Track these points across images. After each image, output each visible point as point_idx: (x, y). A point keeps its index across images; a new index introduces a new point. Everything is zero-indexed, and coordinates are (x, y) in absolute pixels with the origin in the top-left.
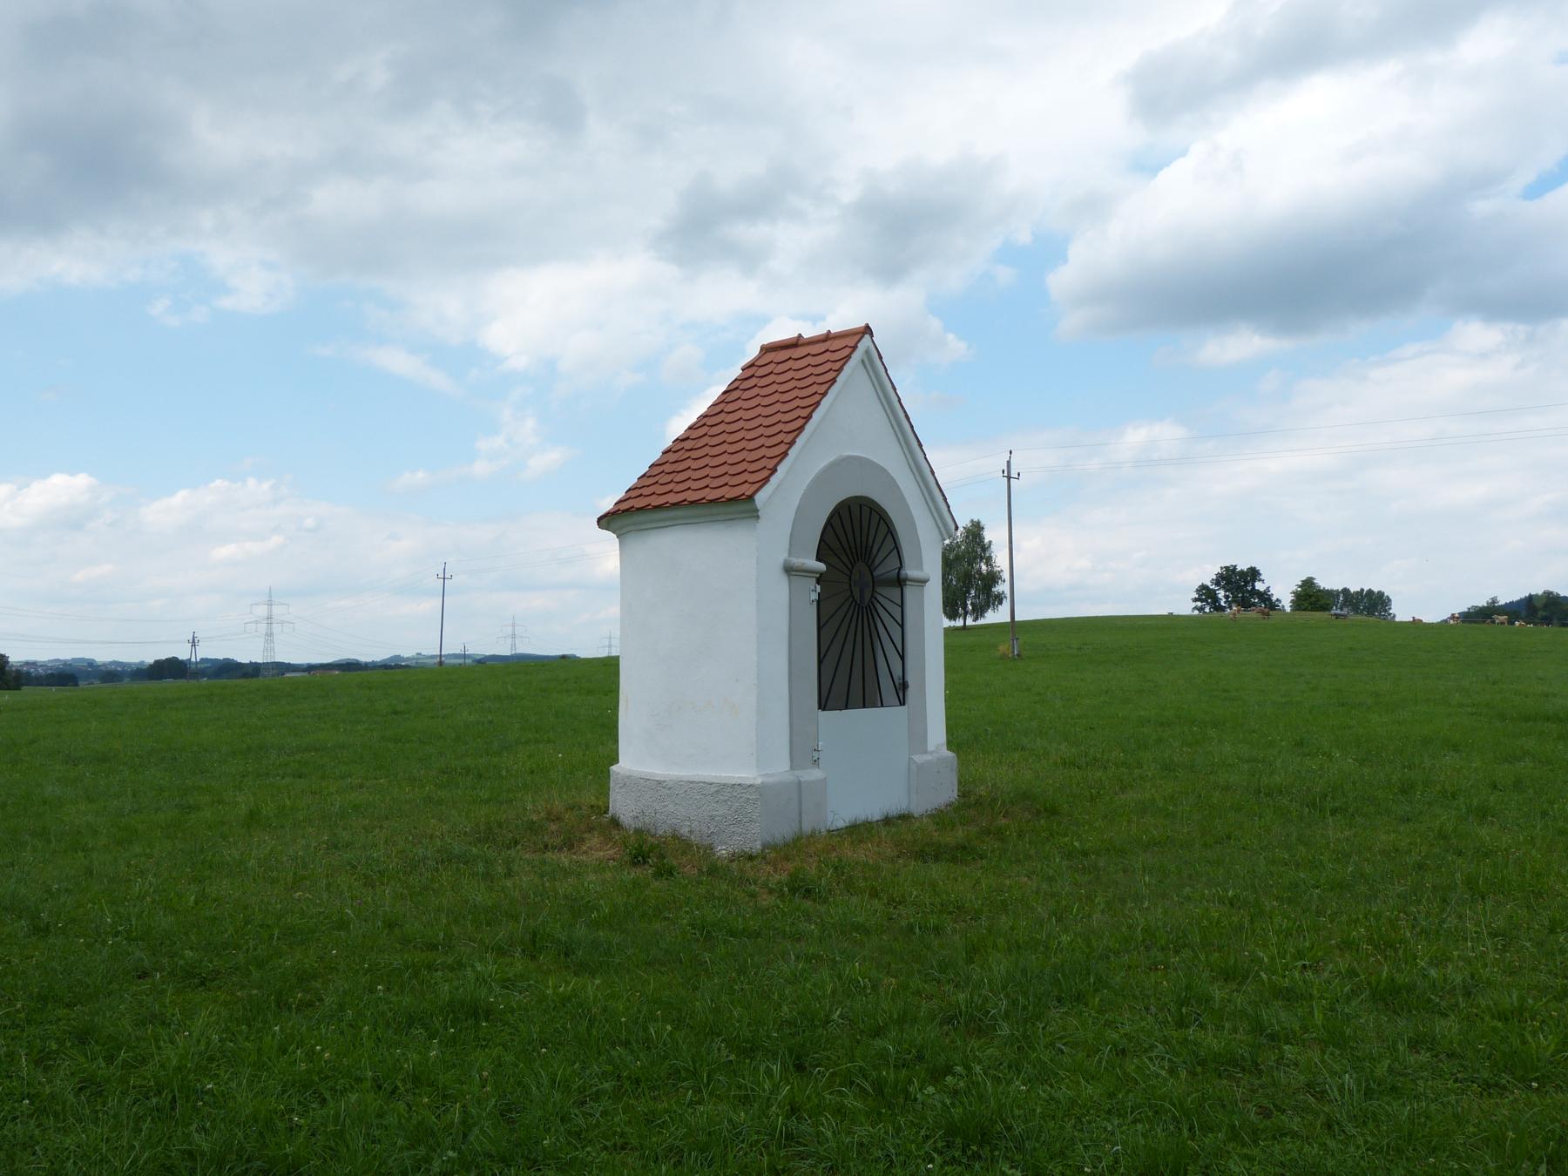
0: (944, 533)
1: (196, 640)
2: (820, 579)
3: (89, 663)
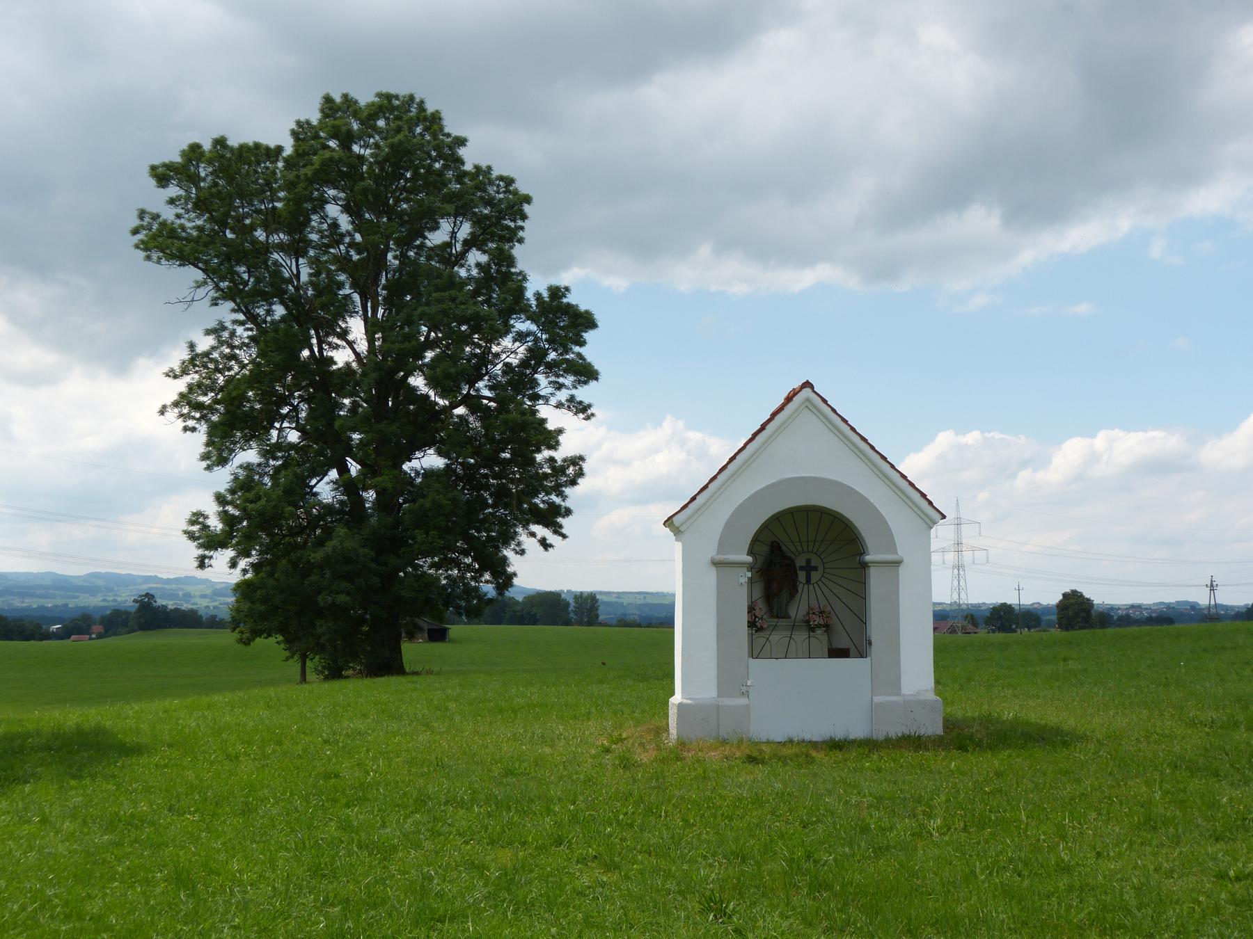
0: (929, 522)
1: (1214, 583)
2: (751, 568)
3: (1191, 606)
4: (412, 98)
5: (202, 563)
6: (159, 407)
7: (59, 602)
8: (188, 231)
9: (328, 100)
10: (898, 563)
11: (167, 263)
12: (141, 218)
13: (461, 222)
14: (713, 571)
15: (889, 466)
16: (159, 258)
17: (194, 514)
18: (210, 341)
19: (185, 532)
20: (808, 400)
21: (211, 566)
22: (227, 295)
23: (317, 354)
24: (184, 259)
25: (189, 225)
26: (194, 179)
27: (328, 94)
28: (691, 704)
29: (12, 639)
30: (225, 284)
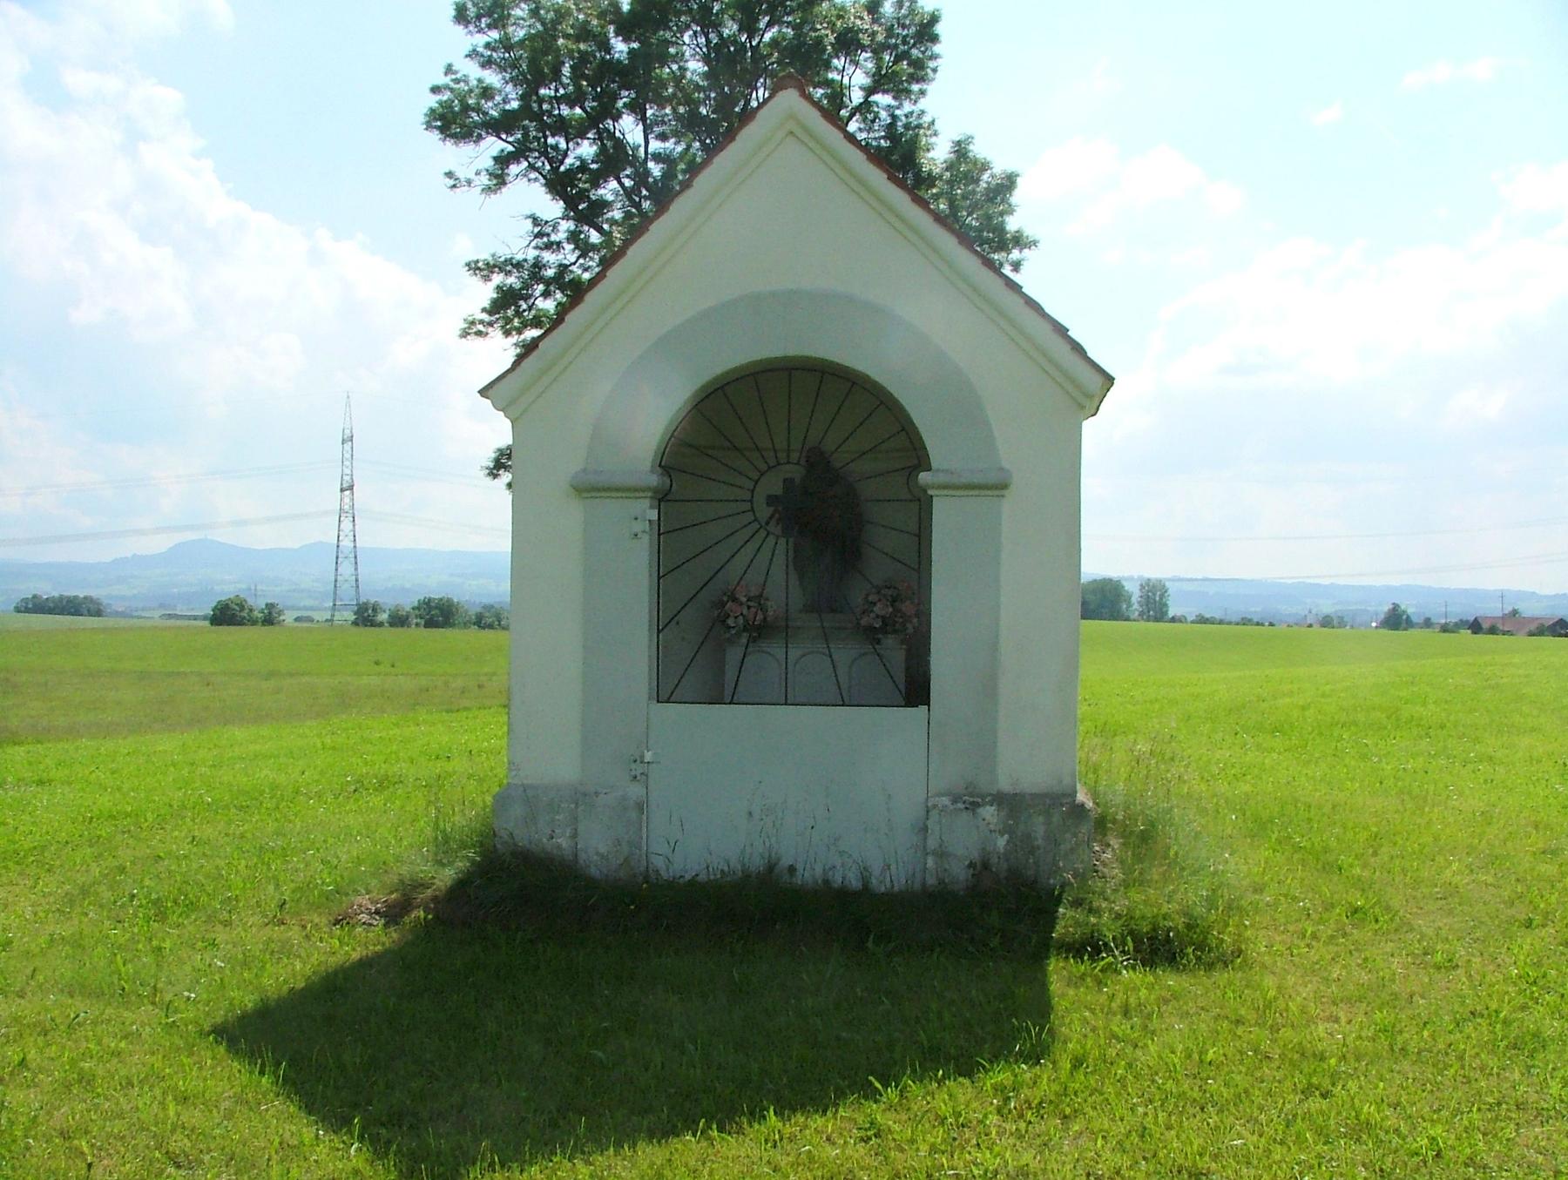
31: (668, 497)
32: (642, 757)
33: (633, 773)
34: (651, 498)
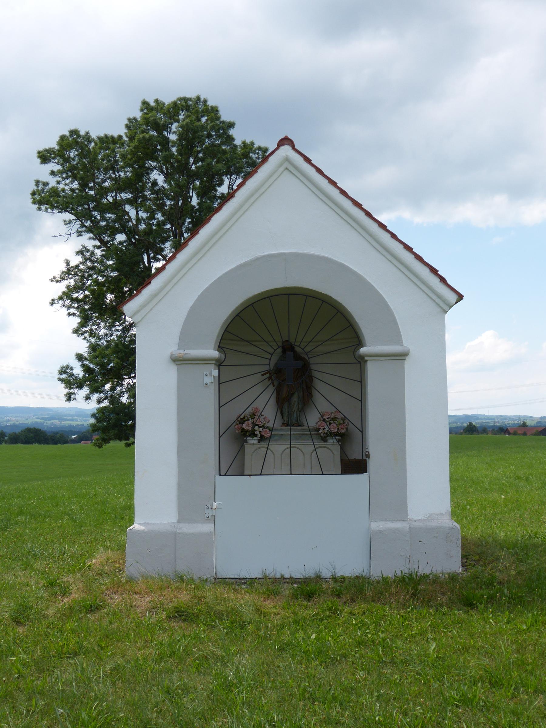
4: (198, 98)
5: (69, 397)
6: (49, 300)
7: (79, 423)
8: (66, 192)
9: (145, 103)
10: (403, 356)
11: (52, 211)
12: (38, 186)
13: (236, 179)
14: (172, 372)
15: (389, 236)
16: (47, 209)
17: (62, 368)
18: (79, 259)
19: (59, 379)
20: (287, 160)
21: (75, 399)
22: (89, 230)
23: (147, 265)
24: (64, 208)
25: (67, 188)
26: (67, 160)
27: (144, 100)
28: (144, 531)
29: (48, 444)
30: (88, 223)
31: (222, 364)
32: (212, 505)
33: (207, 515)
34: (214, 364)
